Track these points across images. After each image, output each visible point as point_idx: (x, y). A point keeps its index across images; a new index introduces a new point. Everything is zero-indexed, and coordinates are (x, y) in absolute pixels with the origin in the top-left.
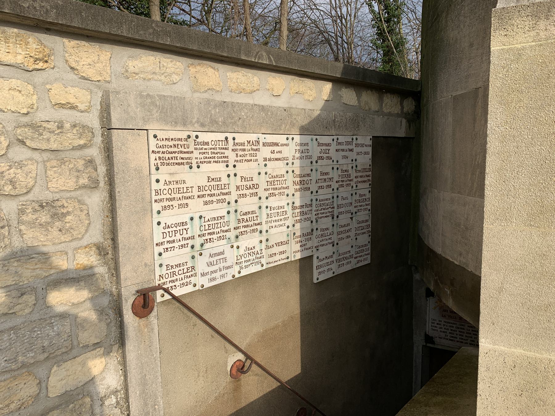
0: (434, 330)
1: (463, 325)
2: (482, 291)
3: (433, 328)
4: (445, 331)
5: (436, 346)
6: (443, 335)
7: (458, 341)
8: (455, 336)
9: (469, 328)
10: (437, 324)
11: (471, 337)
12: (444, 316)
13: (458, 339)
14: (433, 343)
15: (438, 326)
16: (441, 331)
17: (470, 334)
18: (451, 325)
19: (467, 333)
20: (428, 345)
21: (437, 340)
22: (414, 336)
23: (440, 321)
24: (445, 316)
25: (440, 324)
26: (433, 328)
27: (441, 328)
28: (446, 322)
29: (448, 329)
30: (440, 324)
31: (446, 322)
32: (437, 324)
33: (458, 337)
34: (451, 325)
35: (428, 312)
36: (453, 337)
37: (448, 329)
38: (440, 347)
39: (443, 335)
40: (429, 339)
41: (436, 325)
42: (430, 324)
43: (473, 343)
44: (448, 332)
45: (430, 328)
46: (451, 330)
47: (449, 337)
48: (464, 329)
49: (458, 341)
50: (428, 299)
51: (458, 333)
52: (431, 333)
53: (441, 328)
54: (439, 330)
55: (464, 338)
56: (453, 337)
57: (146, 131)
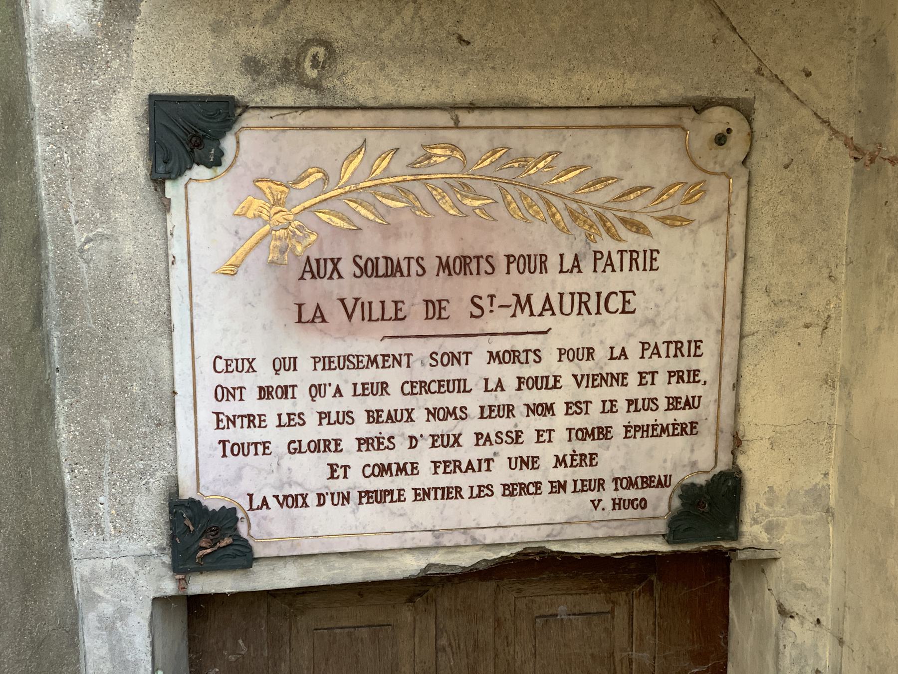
0: (241, 449)
1: (454, 358)
2: (182, 89)
3: (239, 434)
4: (328, 432)
5: (262, 579)
6: (310, 472)
7: (422, 494)
8: (400, 454)
9: (495, 371)
10: (265, 393)
11: (516, 437)
12: (311, 317)
13: (426, 479)
14: (242, 556)
15: (272, 408)
16: (295, 448)
17: (509, 410)
18: (372, 375)
19: (487, 412)
20: (204, 584)
21: (265, 529)
22: (78, 543)
23: (286, 364)
24: (319, 316)
25: (285, 391)
26: (235, 435)
27: (294, 419)
28: (325, 362)
29: (347, 417)
30: (285, 391)
31: (325, 362)
32: (265, 393)
33: (425, 455)
34: (372, 375)
35: (179, 317)
36: (384, 470)
37: (347, 417)
38: (289, 577)
39: (310, 472)
40: (201, 532)
41: (252, 404)
42: (208, 405)
43: (526, 476)
44: (348, 435)
45: (210, 436)
46: (373, 417)
47: (356, 481)
48: (461, 386)
49: (422, 494)
50: (172, 189)
51: (422, 426)
52: (216, 482)
53: (294, 419)
54: (278, 438)
55: (468, 452)
56: (384, 470)
57: (627, 310)
